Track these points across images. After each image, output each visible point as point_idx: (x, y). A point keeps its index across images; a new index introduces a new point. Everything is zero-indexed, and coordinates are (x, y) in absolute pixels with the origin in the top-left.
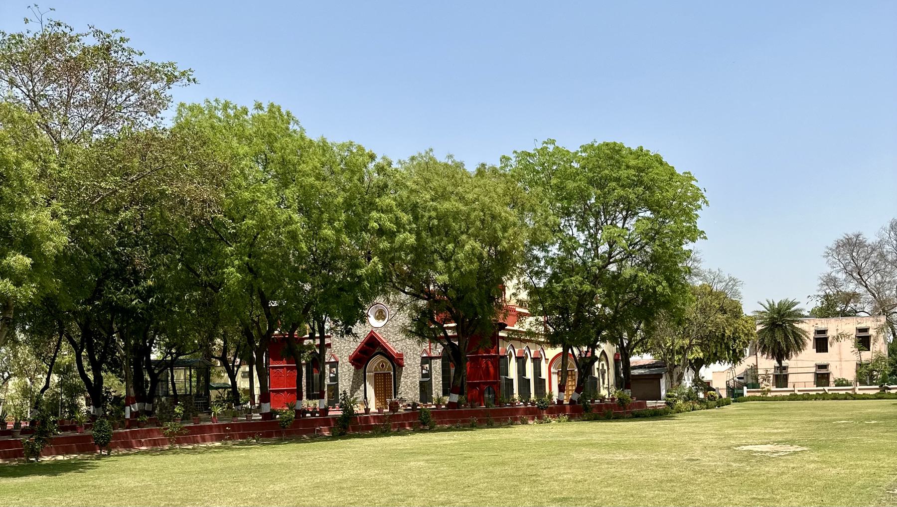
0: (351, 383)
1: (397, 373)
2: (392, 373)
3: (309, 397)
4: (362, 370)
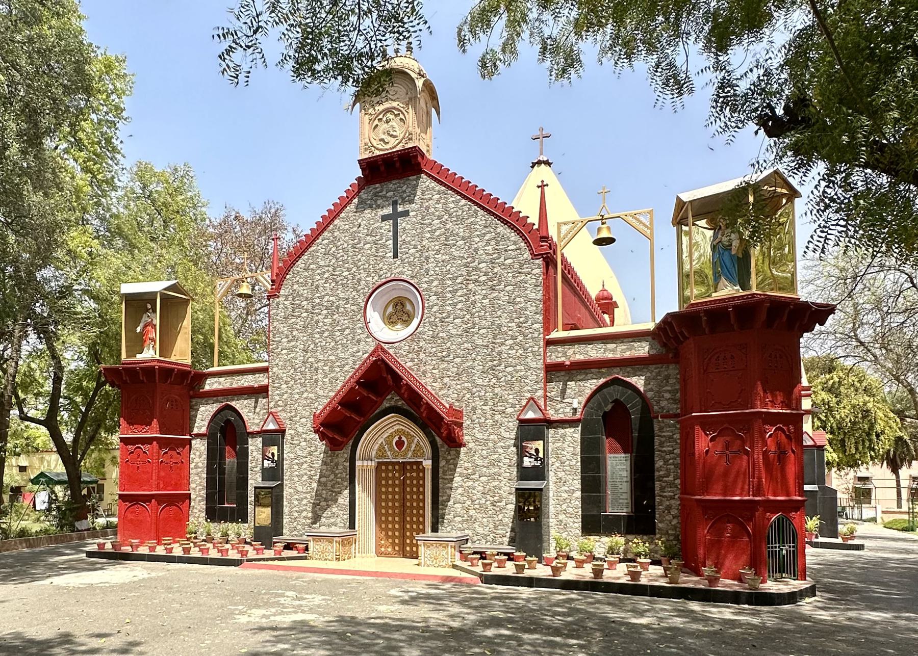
0: (315, 485)
1: (442, 463)
2: (428, 464)
3: (213, 514)
4: (345, 454)
